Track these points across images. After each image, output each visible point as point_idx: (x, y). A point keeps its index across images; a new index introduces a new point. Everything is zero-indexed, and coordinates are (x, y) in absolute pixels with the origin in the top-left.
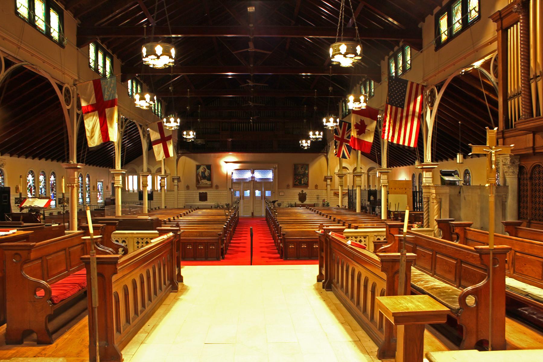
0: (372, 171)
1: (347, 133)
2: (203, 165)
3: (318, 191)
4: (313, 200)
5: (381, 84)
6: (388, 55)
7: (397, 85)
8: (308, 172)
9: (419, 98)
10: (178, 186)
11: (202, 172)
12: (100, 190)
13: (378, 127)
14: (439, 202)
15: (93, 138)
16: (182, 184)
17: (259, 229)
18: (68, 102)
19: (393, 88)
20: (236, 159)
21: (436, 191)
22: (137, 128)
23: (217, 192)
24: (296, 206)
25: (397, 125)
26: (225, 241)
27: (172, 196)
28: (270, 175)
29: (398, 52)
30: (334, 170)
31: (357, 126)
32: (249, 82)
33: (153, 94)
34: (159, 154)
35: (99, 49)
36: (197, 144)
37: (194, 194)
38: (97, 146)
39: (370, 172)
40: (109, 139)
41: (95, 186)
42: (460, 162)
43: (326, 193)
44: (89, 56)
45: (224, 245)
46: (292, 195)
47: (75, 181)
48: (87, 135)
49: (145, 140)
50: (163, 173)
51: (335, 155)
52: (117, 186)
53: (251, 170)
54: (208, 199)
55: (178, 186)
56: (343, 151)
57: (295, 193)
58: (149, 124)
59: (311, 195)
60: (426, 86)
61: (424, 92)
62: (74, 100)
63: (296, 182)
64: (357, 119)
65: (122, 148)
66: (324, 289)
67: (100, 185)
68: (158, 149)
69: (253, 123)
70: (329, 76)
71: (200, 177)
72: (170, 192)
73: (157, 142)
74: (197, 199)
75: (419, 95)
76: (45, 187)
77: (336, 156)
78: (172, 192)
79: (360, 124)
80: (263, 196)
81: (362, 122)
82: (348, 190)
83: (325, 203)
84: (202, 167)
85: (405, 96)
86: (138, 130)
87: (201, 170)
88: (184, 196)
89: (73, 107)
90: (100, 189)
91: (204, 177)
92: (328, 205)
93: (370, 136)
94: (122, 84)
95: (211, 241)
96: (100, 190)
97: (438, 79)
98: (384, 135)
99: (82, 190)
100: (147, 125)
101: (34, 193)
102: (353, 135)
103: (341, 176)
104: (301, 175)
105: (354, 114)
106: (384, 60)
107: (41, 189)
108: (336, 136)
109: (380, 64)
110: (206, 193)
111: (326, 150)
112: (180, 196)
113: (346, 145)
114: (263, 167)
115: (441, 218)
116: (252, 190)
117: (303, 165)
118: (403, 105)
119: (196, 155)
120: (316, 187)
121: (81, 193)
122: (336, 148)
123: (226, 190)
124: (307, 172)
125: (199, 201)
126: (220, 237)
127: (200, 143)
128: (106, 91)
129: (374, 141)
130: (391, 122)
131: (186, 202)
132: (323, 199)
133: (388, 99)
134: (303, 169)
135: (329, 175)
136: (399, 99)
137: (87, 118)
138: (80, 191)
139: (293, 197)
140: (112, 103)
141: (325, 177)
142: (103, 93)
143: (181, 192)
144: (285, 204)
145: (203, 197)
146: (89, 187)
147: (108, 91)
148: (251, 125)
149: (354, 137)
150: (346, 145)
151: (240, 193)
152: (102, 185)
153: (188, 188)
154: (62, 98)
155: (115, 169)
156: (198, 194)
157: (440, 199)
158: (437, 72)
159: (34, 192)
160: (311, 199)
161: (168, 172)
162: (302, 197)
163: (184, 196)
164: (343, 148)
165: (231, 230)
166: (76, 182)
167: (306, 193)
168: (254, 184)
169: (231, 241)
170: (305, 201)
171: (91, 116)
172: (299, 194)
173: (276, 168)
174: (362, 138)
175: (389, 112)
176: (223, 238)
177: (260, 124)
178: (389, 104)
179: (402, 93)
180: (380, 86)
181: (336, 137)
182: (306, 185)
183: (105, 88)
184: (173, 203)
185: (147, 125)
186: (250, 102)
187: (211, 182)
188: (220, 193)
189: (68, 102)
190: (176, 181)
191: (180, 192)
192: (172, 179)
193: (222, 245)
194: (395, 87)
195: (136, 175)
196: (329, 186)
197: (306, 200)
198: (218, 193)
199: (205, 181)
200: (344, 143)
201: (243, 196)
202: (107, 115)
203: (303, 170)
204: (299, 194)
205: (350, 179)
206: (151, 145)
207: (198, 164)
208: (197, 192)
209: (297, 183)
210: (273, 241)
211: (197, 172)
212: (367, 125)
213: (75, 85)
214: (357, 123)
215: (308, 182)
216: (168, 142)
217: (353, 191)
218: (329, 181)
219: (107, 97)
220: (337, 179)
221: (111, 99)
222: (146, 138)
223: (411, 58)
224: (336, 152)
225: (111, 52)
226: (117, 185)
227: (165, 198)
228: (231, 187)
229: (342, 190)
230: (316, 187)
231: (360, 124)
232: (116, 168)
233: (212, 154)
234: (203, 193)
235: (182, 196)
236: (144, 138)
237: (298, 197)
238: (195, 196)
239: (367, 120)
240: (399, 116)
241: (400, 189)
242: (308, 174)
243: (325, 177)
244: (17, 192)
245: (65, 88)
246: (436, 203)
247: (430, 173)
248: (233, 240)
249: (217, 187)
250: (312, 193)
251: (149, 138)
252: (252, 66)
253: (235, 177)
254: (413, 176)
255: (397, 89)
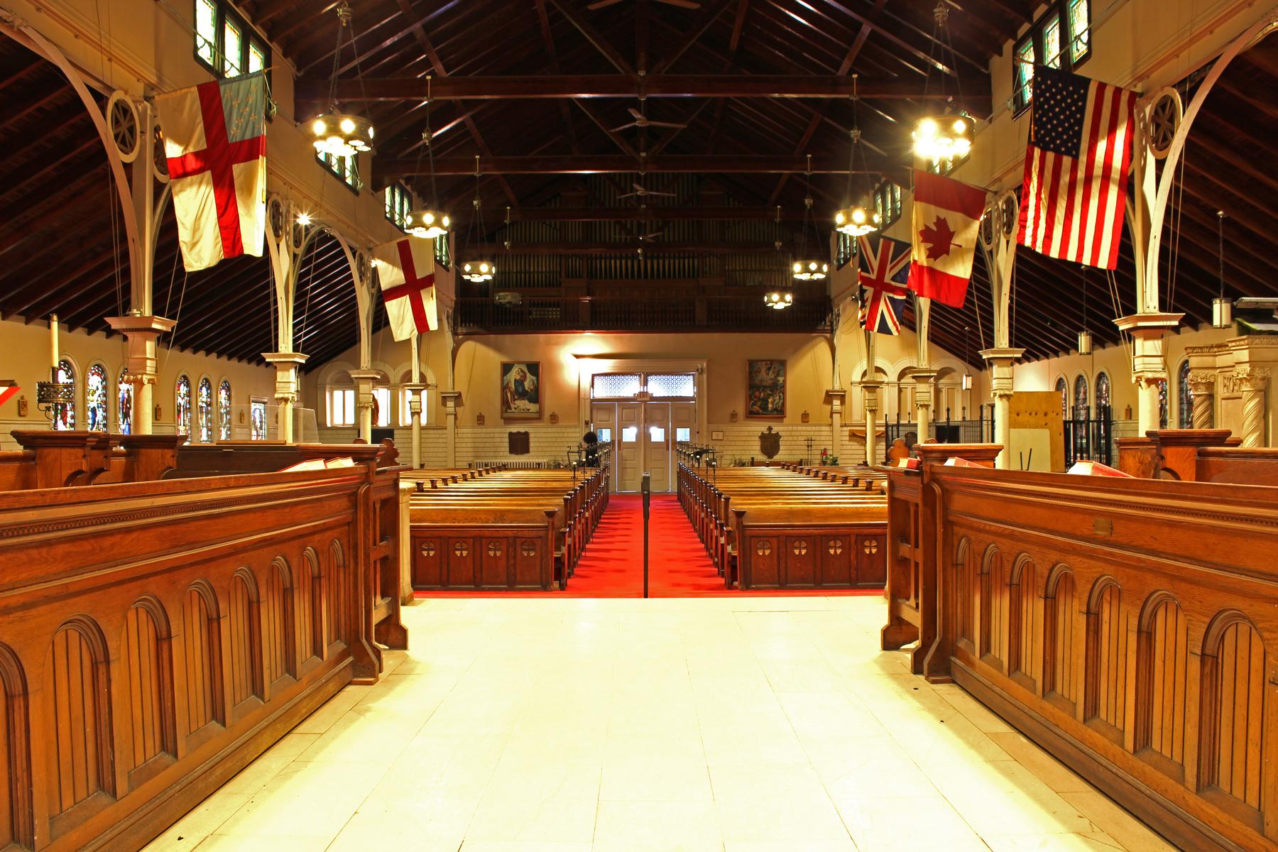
0: (946, 377)
1: (891, 269)
2: (520, 363)
3: (809, 428)
4: (798, 452)
5: (990, 121)
6: (1014, 36)
7: (1059, 91)
8: (785, 381)
9: (1121, 134)
10: (455, 415)
11: (516, 381)
12: (258, 424)
13: (983, 241)
14: (1260, 391)
15: (198, 246)
16: (466, 412)
17: (662, 520)
18: (126, 142)
19: (1047, 101)
20: (606, 349)
21: (1251, 355)
22: (342, 253)
23: (554, 430)
24: (753, 463)
25: (1058, 205)
26: (569, 541)
27: (441, 440)
28: (685, 387)
29: (1045, 19)
30: (850, 375)
31: (926, 235)
32: (638, 116)
33: (364, 120)
34: (402, 322)
35: (227, 17)
36: (500, 303)
37: (497, 435)
38: (208, 271)
39: (942, 381)
40: (242, 248)
41: (245, 412)
42: (1224, 323)
43: (829, 433)
44: (195, 26)
45: (564, 549)
46: (744, 438)
47: (145, 367)
48: (181, 239)
49: (365, 285)
50: (416, 379)
51: (862, 324)
52: (282, 399)
53: (640, 376)
54: (531, 449)
55: (455, 415)
56: (882, 314)
57: (751, 434)
58: (377, 246)
59: (791, 438)
60: (1141, 95)
61: (1135, 111)
62: (145, 140)
63: (753, 404)
64: (926, 215)
65: (296, 299)
66: (922, 677)
67: (258, 411)
68: (399, 310)
69: (645, 257)
70: (852, 101)
71: (511, 392)
72: (436, 431)
73: (395, 292)
74: (503, 449)
75: (1122, 123)
76: (105, 405)
77: (864, 327)
78: (440, 431)
79: (934, 228)
80: (671, 441)
81: (941, 223)
82: (887, 425)
83: (827, 458)
84: (515, 370)
85: (1080, 123)
86: (346, 260)
87: (514, 375)
88: (471, 440)
89: (141, 157)
90: (258, 420)
91: (522, 394)
92: (834, 462)
93: (963, 261)
94: (296, 126)
95: (527, 533)
96: (258, 424)
97: (1184, 66)
98: (1024, 234)
99: (208, 420)
100: (370, 249)
101: (73, 421)
102: (916, 259)
103: (871, 387)
104: (765, 387)
105: (918, 203)
106: (1001, 54)
107: (94, 411)
108: (863, 274)
109: (987, 66)
110: (526, 434)
111: (828, 323)
112: (462, 440)
113: (889, 297)
114: (670, 366)
115: (1266, 445)
116: (642, 425)
117: (772, 362)
118: (1077, 147)
119: (501, 337)
120: (805, 417)
121: (207, 427)
122: (863, 306)
123: (575, 427)
124: (781, 379)
125: (507, 453)
126: (551, 520)
127: (509, 303)
128: (235, 116)
129: (972, 275)
130: (1043, 196)
131: (477, 457)
132: (823, 448)
133: (1035, 131)
134: (771, 372)
135: (837, 387)
136: (1065, 131)
137: (182, 190)
138: (204, 422)
139: (747, 443)
140: (250, 150)
141: (827, 392)
142: (226, 120)
143: (465, 430)
144: (726, 461)
145: (519, 444)
146: (228, 413)
147: (241, 115)
148: (639, 261)
149: (919, 263)
150: (889, 297)
151: (612, 434)
152: (263, 411)
153: (481, 420)
154: (105, 129)
155: (277, 350)
156: (507, 435)
157: (1263, 379)
158: (1187, 40)
159: (73, 417)
160: (791, 448)
161: (431, 379)
162: (770, 444)
163: (471, 440)
164: (882, 307)
165: (587, 514)
166: (148, 369)
167: (780, 433)
168: (647, 408)
169: (587, 546)
170: (776, 453)
171: (191, 185)
172: (763, 437)
173: (702, 369)
174: (939, 266)
175: (1037, 170)
176: (562, 530)
177: (661, 262)
178: (1036, 144)
179: (1073, 115)
180: (990, 126)
181: (862, 278)
182: (780, 413)
183: (232, 106)
184: (443, 459)
185: (370, 249)
186: (635, 186)
187: (540, 408)
188: (561, 435)
189: (126, 142)
190: (451, 404)
191: (460, 431)
192: (440, 399)
193: (558, 549)
194: (1053, 96)
195: (351, 389)
196: (836, 417)
197: (780, 452)
198: (557, 435)
199: (523, 404)
200: (884, 292)
201: (620, 441)
202: (237, 183)
203: (771, 375)
204: (763, 437)
205: (889, 399)
206: (381, 297)
207: (505, 359)
208: (502, 430)
209: (756, 408)
210: (703, 546)
211: (502, 380)
212: (954, 233)
213: (148, 99)
214: (926, 226)
215: (783, 404)
216: (424, 294)
217: (900, 428)
218: (837, 402)
219: (236, 132)
220: (858, 396)
221: (248, 136)
222: (367, 282)
223: (1089, 21)
224: (863, 317)
225: (266, 34)
226: (281, 396)
227: (421, 438)
228: (588, 419)
229: (874, 425)
230: (805, 417)
231: (934, 228)
232: (280, 349)
233: (542, 337)
234: (518, 433)
235: (466, 440)
236: (361, 281)
237: (759, 444)
238: (498, 440)
239: (954, 218)
240: (1065, 179)
241: (1030, 414)
242: (783, 386)
243: (827, 392)
244: (22, 413)
245: (116, 105)
246: (1251, 394)
247: (1156, 342)
248: (593, 543)
249: (554, 418)
250: (793, 433)
251: (377, 285)
252: (642, 73)
253: (603, 390)
254: (1060, 384)
255: (1058, 104)
